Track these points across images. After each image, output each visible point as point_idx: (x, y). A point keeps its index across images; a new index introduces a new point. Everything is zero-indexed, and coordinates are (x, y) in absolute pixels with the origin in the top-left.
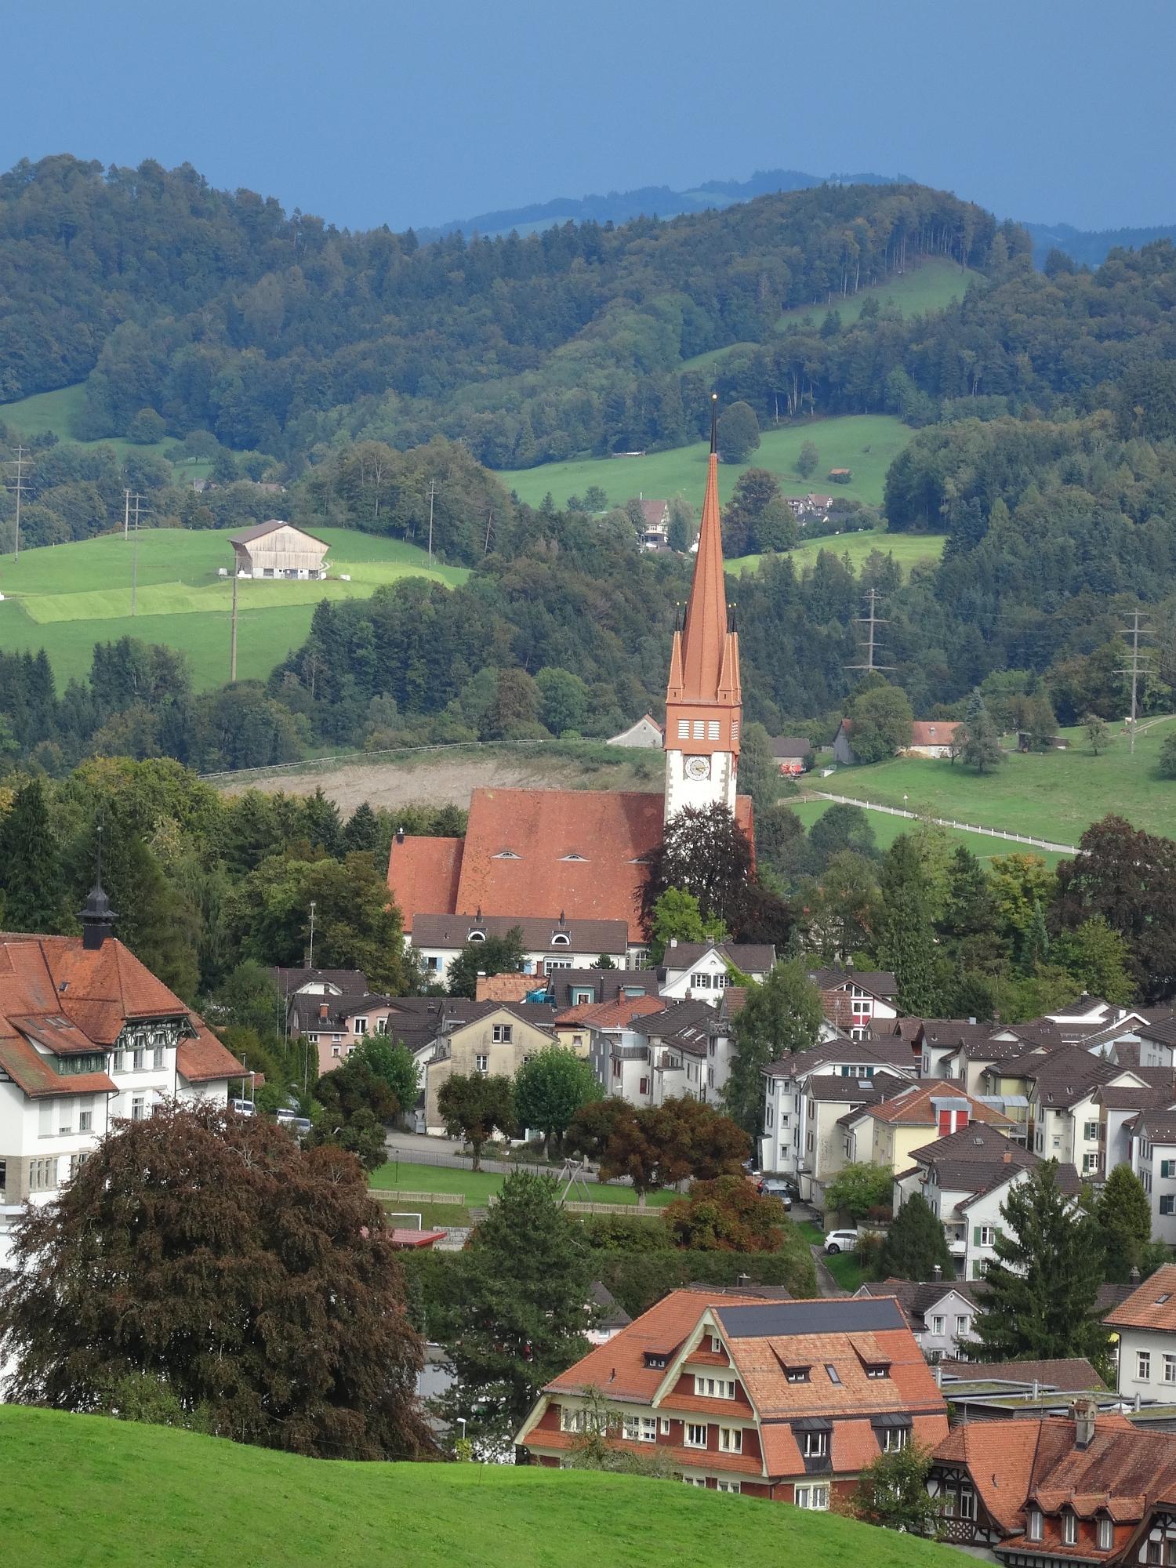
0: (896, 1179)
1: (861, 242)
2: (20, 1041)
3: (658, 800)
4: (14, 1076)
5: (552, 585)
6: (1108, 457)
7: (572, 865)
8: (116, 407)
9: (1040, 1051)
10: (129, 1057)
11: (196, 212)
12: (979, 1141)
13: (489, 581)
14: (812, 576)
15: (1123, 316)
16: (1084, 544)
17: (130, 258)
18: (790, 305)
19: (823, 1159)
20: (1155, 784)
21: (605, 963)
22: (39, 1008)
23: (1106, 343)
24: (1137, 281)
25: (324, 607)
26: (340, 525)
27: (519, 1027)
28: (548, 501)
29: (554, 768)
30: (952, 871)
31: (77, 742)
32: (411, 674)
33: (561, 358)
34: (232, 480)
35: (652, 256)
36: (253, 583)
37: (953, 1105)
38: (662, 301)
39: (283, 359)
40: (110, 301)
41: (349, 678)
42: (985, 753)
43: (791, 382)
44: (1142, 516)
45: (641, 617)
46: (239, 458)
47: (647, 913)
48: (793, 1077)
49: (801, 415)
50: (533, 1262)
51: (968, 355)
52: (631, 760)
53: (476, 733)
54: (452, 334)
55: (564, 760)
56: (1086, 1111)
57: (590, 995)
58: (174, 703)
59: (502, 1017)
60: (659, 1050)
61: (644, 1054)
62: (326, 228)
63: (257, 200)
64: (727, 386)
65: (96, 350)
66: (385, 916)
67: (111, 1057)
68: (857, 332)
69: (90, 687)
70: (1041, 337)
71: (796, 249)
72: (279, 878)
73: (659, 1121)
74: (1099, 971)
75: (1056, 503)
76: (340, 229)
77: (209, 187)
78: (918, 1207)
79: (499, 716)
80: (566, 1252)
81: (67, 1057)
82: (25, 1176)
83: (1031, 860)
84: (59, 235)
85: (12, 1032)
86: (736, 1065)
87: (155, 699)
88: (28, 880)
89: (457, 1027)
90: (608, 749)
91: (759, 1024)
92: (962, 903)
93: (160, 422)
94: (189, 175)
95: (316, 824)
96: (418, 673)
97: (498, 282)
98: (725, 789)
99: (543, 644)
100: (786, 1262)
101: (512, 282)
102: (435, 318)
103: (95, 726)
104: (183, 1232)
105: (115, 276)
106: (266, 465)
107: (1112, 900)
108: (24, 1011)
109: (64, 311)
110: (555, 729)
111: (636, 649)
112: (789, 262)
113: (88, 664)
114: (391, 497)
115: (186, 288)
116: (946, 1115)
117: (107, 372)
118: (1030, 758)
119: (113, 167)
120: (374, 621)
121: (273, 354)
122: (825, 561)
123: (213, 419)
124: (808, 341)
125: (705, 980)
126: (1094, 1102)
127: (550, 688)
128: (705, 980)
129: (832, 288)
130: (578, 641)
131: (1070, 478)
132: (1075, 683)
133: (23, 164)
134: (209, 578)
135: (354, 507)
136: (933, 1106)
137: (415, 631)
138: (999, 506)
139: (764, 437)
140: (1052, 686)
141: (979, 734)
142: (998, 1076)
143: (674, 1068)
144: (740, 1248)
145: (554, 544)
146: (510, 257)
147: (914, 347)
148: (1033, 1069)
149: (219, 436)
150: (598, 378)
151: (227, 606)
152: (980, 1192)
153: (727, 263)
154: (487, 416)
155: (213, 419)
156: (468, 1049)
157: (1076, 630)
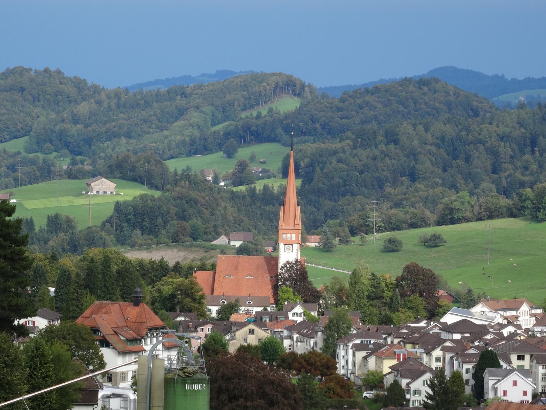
0: (385, 375)
1: (265, 90)
2: (116, 335)
3: (276, 259)
4: (115, 346)
5: (187, 195)
6: (350, 154)
7: (250, 279)
8: (38, 143)
9: (416, 335)
10: (149, 340)
11: (61, 83)
12: (411, 363)
13: (168, 194)
14: (262, 192)
15: (348, 112)
16: (345, 181)
17: (41, 97)
18: (244, 110)
19: (359, 369)
20: (382, 254)
21: (265, 310)
22: (120, 325)
23: (343, 120)
24: (352, 101)
25: (118, 202)
26: (118, 178)
27: (257, 329)
28: (176, 170)
29: (195, 251)
30: (370, 279)
31: (43, 245)
32: (145, 223)
33: (175, 127)
34: (76, 165)
35: (201, 95)
36: (94, 196)
37: (401, 352)
38: (205, 109)
39: (90, 128)
40: (36, 111)
41: (125, 225)
42: (329, 245)
43: (247, 133)
44: (362, 172)
45: (214, 205)
46: (78, 158)
47: (275, 294)
48: (346, 344)
49: (251, 143)
50: (308, 403)
51: (301, 124)
52: (219, 248)
53: (171, 241)
54: (141, 120)
55: (199, 248)
56: (437, 353)
57: (268, 319)
58: (72, 233)
59: (251, 326)
60: (295, 336)
61: (291, 337)
62: (101, 88)
63: (80, 79)
64: (227, 135)
65: (32, 126)
66: (200, 296)
67: (143, 340)
68: (266, 118)
69: (46, 228)
70: (323, 118)
71: (246, 93)
72: (167, 284)
73: (310, 358)
74: (417, 310)
75: (335, 169)
76: (105, 88)
77: (65, 76)
78: (396, 384)
79: (178, 236)
80: (318, 399)
81: (130, 341)
82: (118, 378)
83: (388, 276)
84: (19, 91)
85: (113, 333)
86: (325, 341)
87: (66, 232)
88: (105, 286)
89: (237, 330)
90: (212, 245)
91: (333, 327)
92: (374, 290)
93: (52, 148)
94: (59, 72)
95: (162, 268)
96: (147, 223)
97: (154, 104)
98: (297, 255)
99: (185, 213)
100: (356, 402)
101: (159, 104)
102: (136, 115)
103: (48, 241)
104: (235, 394)
105: (37, 103)
106: (85, 160)
107: (413, 288)
108: (116, 326)
109: (22, 114)
110: (195, 239)
111: (213, 215)
112: (243, 96)
113: (45, 221)
114: (133, 169)
115: (59, 107)
116: (399, 355)
117: (35, 132)
118: (342, 246)
119: (36, 70)
120: (133, 207)
121: (86, 126)
122: (266, 187)
123: (68, 147)
124: (252, 120)
125: (297, 315)
126: (441, 350)
127: (193, 226)
128: (297, 315)
129: (257, 104)
130: (196, 212)
131: (340, 161)
132: (355, 224)
133: (8, 69)
134: (79, 195)
135: (121, 171)
136: (395, 352)
137: (146, 210)
138: (318, 170)
139: (239, 150)
140: (347, 224)
141: (327, 239)
142: (405, 343)
143: (301, 342)
144: (341, 397)
145: (187, 182)
146: (158, 97)
147: (284, 122)
148: (416, 340)
149: (70, 151)
150: (187, 133)
151: (88, 203)
152: (414, 379)
153: (224, 97)
154: (154, 144)
155: (68, 147)
156: (241, 336)
157: (345, 207)
